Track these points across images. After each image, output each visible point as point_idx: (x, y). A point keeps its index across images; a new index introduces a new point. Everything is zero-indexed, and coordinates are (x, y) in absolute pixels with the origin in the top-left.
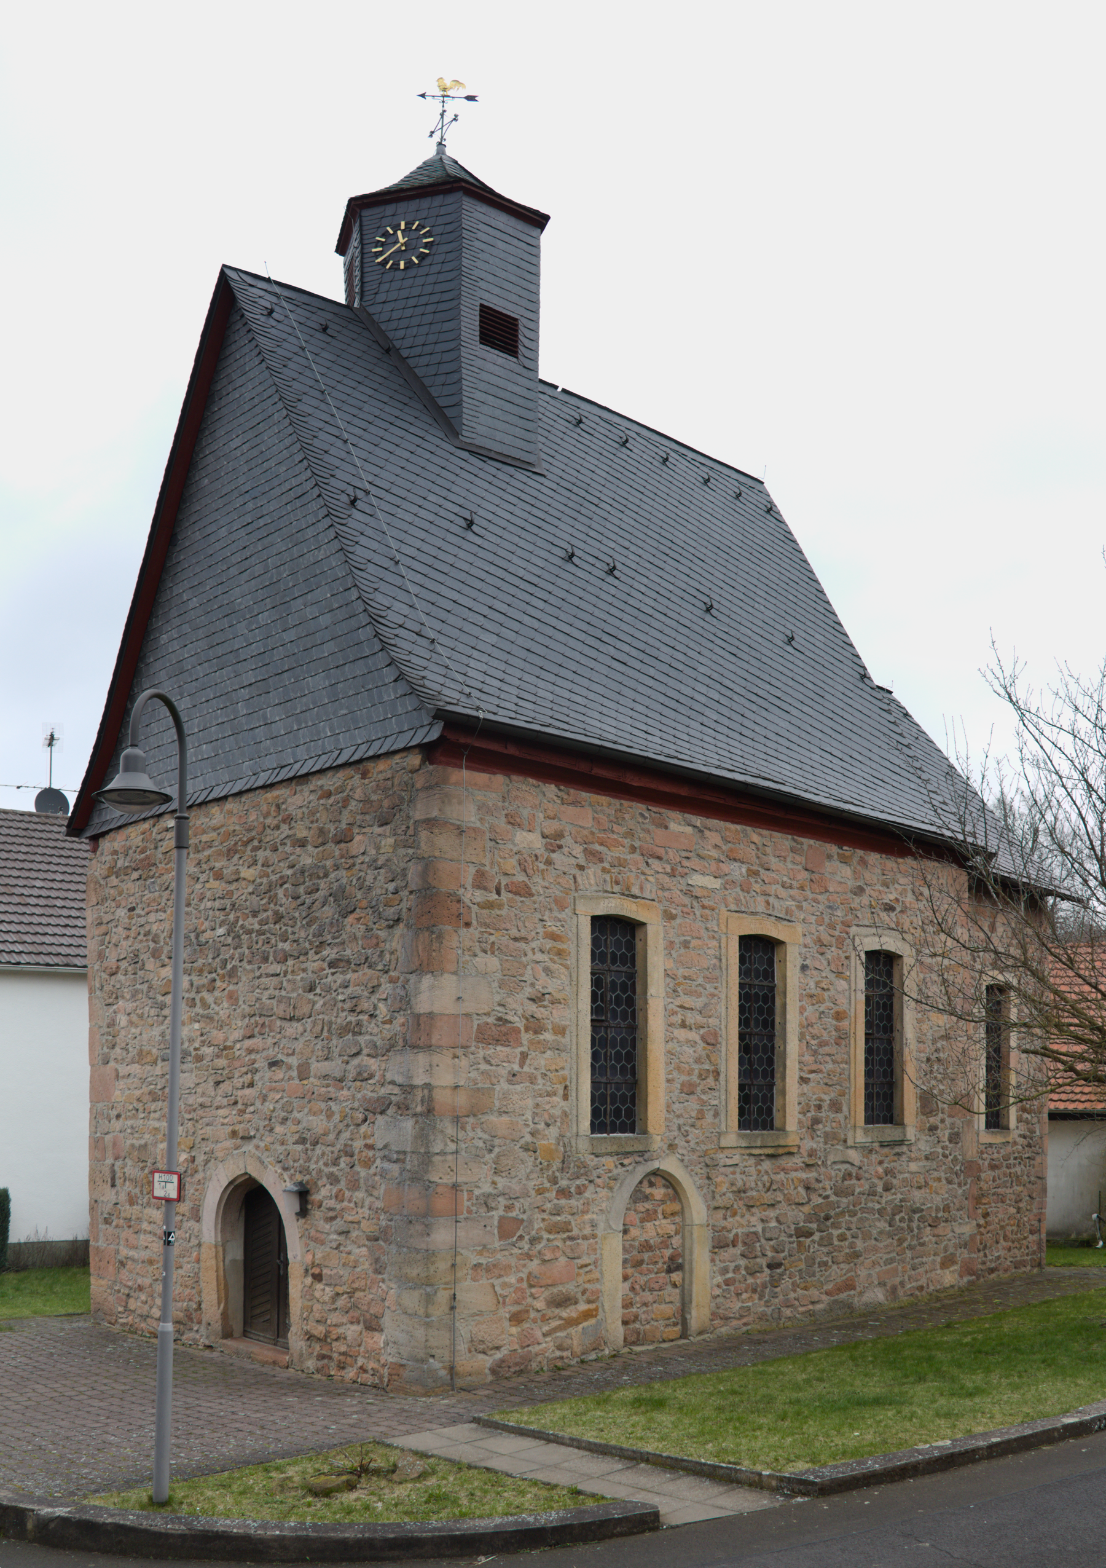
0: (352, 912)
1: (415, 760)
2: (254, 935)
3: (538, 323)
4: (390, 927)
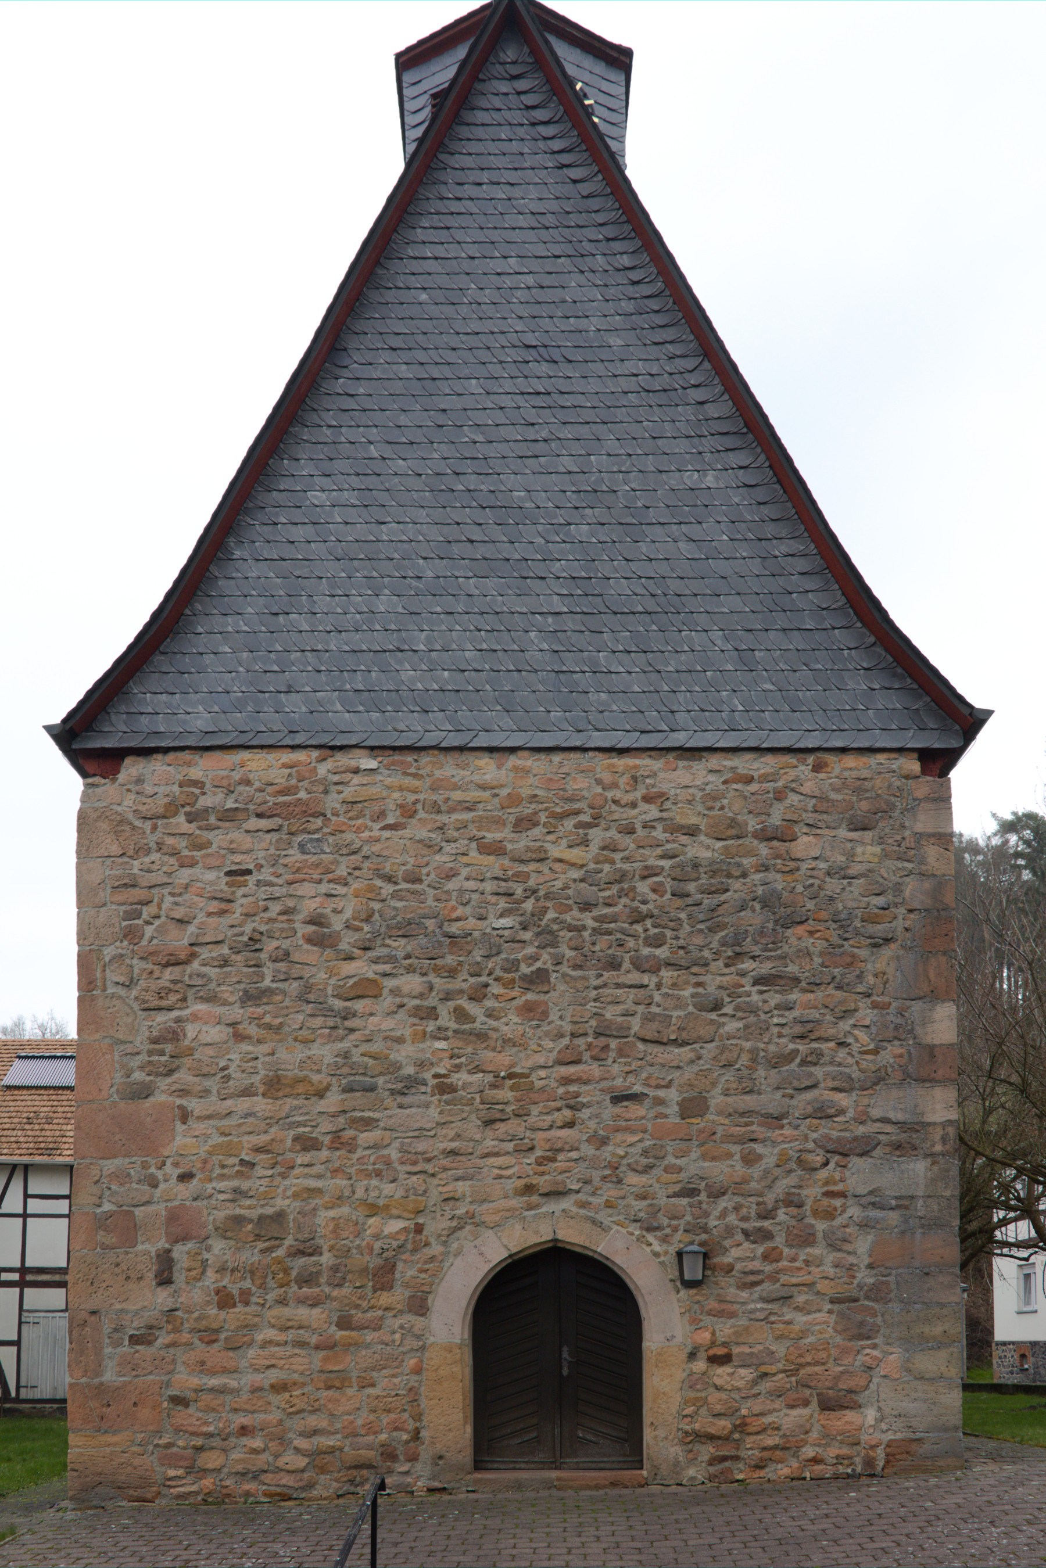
0: (801, 923)
1: (916, 767)
2: (586, 934)
3: (623, 142)
4: (875, 946)
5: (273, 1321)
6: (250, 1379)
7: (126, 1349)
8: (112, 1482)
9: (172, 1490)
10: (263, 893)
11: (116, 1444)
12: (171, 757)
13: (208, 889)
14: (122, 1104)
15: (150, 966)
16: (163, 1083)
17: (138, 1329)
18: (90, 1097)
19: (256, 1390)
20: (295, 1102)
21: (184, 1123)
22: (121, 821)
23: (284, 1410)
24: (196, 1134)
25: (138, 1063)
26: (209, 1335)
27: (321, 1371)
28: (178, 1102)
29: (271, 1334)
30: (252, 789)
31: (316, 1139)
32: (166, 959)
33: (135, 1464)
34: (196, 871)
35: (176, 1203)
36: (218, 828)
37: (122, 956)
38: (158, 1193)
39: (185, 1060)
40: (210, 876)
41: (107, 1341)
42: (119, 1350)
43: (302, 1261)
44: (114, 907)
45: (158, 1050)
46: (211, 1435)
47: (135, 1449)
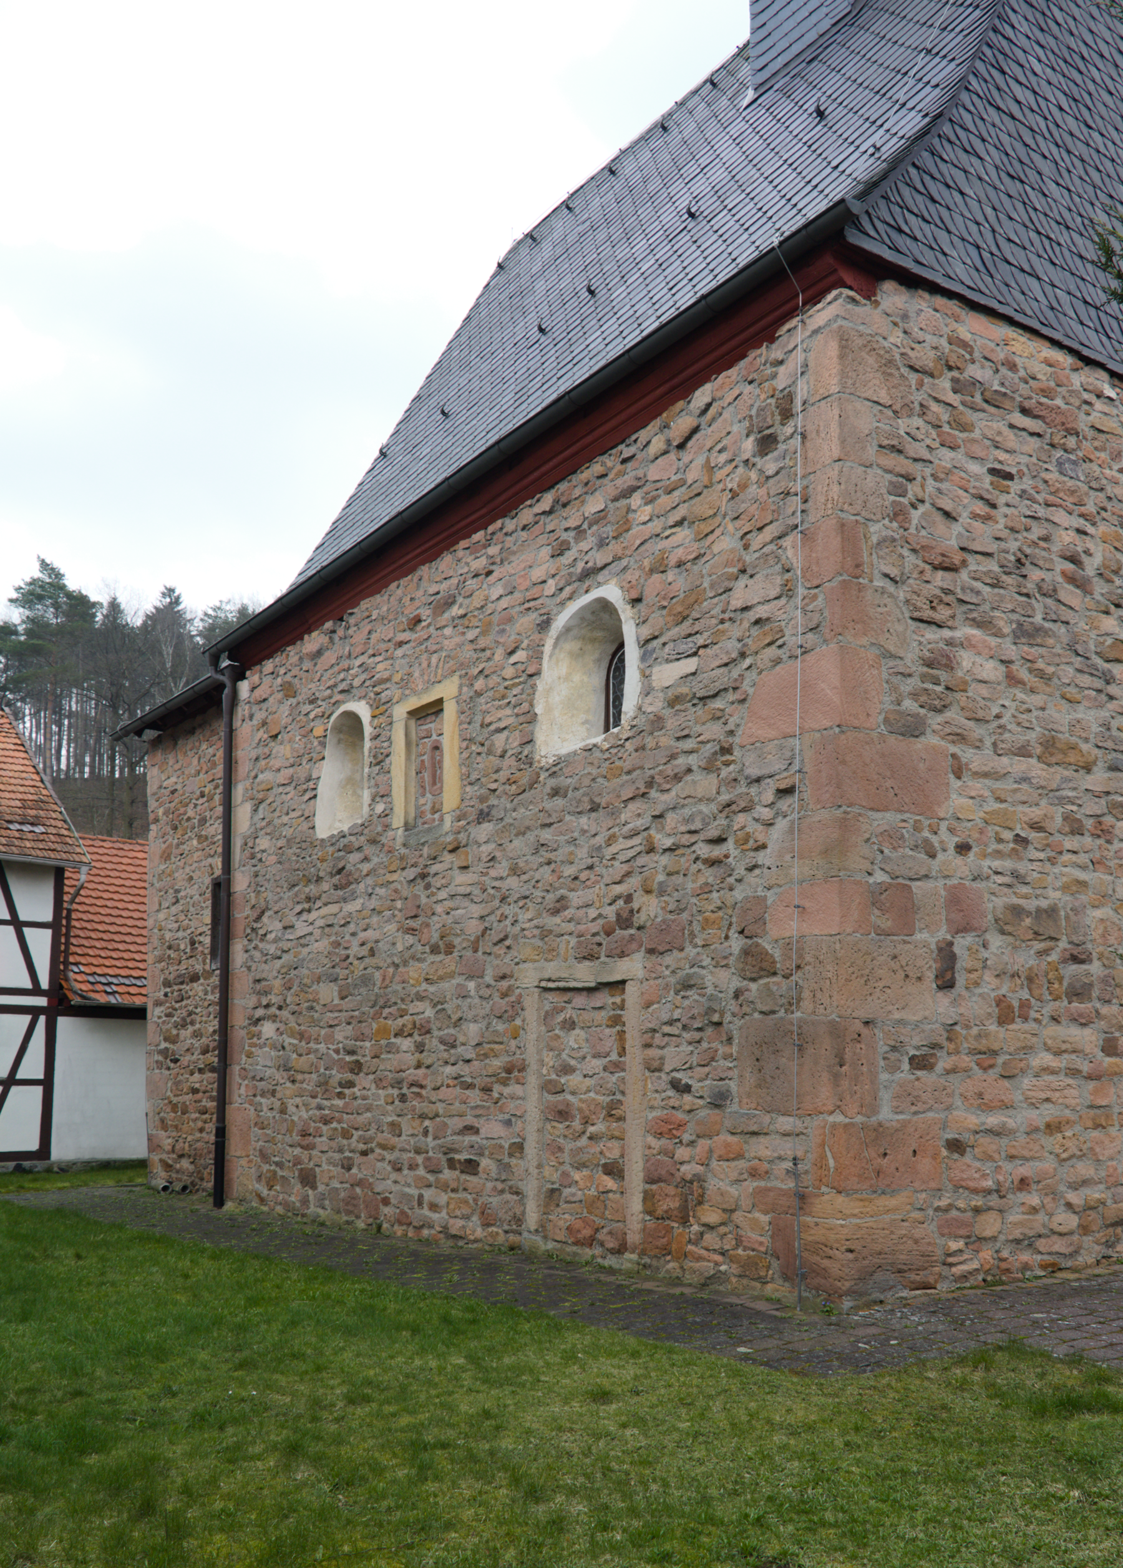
5: (1049, 1042)
6: (1019, 1119)
7: (905, 1072)
8: (892, 1264)
9: (954, 1270)
10: (1024, 507)
11: (895, 1210)
12: (940, 301)
13: (973, 483)
14: (892, 740)
15: (922, 565)
16: (935, 721)
17: (918, 1048)
18: (856, 723)
19: (1033, 1131)
20: (1066, 773)
21: (959, 778)
22: (890, 361)
23: (1057, 1155)
24: (973, 794)
25: (908, 689)
26: (986, 1056)
27: (1091, 1107)
28: (953, 749)
29: (1046, 1059)
30: (1016, 377)
31: (1079, 821)
32: (940, 559)
33: (917, 1236)
34: (959, 456)
35: (955, 881)
36: (984, 411)
37: (894, 540)
38: (935, 864)
39: (958, 695)
40: (975, 468)
41: (882, 1063)
42: (898, 1076)
43: (1074, 968)
44: (879, 471)
45: (933, 676)
46: (988, 1192)
47: (916, 1215)
